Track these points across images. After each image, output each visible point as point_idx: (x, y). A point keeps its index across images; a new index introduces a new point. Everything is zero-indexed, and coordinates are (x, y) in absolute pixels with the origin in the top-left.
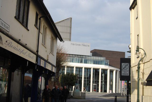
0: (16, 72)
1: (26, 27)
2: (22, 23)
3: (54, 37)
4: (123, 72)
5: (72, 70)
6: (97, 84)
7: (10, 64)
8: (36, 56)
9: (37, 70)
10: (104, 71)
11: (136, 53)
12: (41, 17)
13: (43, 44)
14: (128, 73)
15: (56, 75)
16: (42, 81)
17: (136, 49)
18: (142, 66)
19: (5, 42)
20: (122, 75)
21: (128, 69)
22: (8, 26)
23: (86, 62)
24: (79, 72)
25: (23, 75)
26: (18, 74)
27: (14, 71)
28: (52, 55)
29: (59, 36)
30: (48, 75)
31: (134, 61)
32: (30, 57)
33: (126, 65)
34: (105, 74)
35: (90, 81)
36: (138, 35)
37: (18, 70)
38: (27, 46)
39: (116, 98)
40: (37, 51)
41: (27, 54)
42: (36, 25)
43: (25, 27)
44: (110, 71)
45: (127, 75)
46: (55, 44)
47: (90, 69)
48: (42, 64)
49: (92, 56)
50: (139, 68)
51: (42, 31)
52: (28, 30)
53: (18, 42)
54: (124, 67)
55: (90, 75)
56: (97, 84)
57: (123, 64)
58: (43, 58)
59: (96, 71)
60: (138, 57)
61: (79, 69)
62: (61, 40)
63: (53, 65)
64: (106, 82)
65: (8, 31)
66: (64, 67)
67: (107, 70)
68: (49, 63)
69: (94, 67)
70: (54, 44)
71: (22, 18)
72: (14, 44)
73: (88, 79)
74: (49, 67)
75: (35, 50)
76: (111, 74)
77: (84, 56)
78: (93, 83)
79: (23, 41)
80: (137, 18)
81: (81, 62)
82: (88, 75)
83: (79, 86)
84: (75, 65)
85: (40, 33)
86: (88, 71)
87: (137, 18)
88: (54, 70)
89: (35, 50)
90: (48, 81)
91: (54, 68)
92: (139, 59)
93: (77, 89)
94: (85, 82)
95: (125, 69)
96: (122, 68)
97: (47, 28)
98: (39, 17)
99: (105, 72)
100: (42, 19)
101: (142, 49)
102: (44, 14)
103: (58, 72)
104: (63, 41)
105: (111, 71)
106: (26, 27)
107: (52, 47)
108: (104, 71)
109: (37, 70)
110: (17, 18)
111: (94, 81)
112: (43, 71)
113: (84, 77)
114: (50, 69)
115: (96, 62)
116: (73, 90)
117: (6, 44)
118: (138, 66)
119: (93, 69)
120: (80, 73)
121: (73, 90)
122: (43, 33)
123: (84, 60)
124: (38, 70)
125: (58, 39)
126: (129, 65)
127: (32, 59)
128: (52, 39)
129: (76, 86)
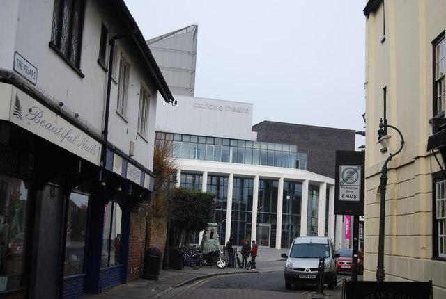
0: (47, 190)
1: (76, 67)
2: (66, 59)
3: (148, 91)
4: (342, 191)
5: (197, 182)
6: (270, 225)
7: (32, 169)
8: (100, 145)
9: (104, 184)
10: (292, 186)
11: (379, 138)
12: (114, 38)
13: (120, 112)
14: (357, 192)
15: (152, 196)
16: (115, 215)
17: (379, 129)
18: (392, 177)
19: (27, 112)
20: (341, 198)
21: (358, 183)
22: (34, 70)
23: (238, 159)
24: (218, 189)
25: (65, 197)
26: (52, 196)
27: (42, 188)
28: (143, 141)
29: (161, 87)
30: (131, 196)
31: (373, 162)
32: (85, 148)
33: (352, 170)
34: (295, 193)
35: (250, 216)
36: (385, 89)
37: (53, 184)
38: (62, 107)
39: (323, 263)
40: (105, 132)
41: (79, 141)
42: (100, 62)
43: (74, 69)
44: (309, 185)
45: (353, 199)
46: (151, 110)
47: (251, 178)
48: (117, 169)
49: (258, 141)
50: (384, 180)
51: (116, 75)
52: (82, 76)
53: (57, 110)
54: (345, 175)
55: (251, 198)
56: (270, 225)
57: (342, 168)
58: (120, 151)
59: (269, 185)
60: (384, 151)
61: (218, 179)
62: (168, 97)
63: (144, 170)
64: (297, 219)
65: (34, 82)
66: (175, 172)
67: (300, 182)
68: (136, 164)
69: (260, 172)
70: (148, 106)
71: (66, 48)
72: (49, 115)
73: (242, 209)
74: (133, 176)
75: (97, 128)
76: (313, 194)
77: (232, 141)
78: (259, 221)
79: (70, 108)
80: (383, 41)
81: (224, 159)
82: (246, 198)
83: (219, 228)
84: (207, 166)
85: (112, 83)
86: (246, 184)
87: (383, 41)
88: (148, 183)
89: (97, 128)
90: (132, 214)
91: (147, 177)
92: (387, 156)
93: (211, 237)
94: (236, 218)
95: (348, 181)
96: (341, 180)
97: (129, 65)
98: (108, 38)
99: (294, 188)
100: (117, 42)
101: (397, 130)
102: (123, 33)
103: (157, 185)
104: (173, 99)
105: (314, 187)
106: (76, 67)
107: (142, 121)
108: (292, 186)
109: (104, 184)
110: (54, 46)
111: (263, 216)
112: (130, 196)
113: (232, 212)
114: (138, 182)
115: (268, 160)
116: (200, 242)
117: (31, 116)
118: (381, 174)
119: (261, 179)
120: (221, 191)
121: (200, 242)
122: (111, 67)
123: (234, 155)
124: (103, 183)
125: (159, 95)
126: (359, 171)
127: (89, 152)
128: (144, 96)
129: (210, 229)
